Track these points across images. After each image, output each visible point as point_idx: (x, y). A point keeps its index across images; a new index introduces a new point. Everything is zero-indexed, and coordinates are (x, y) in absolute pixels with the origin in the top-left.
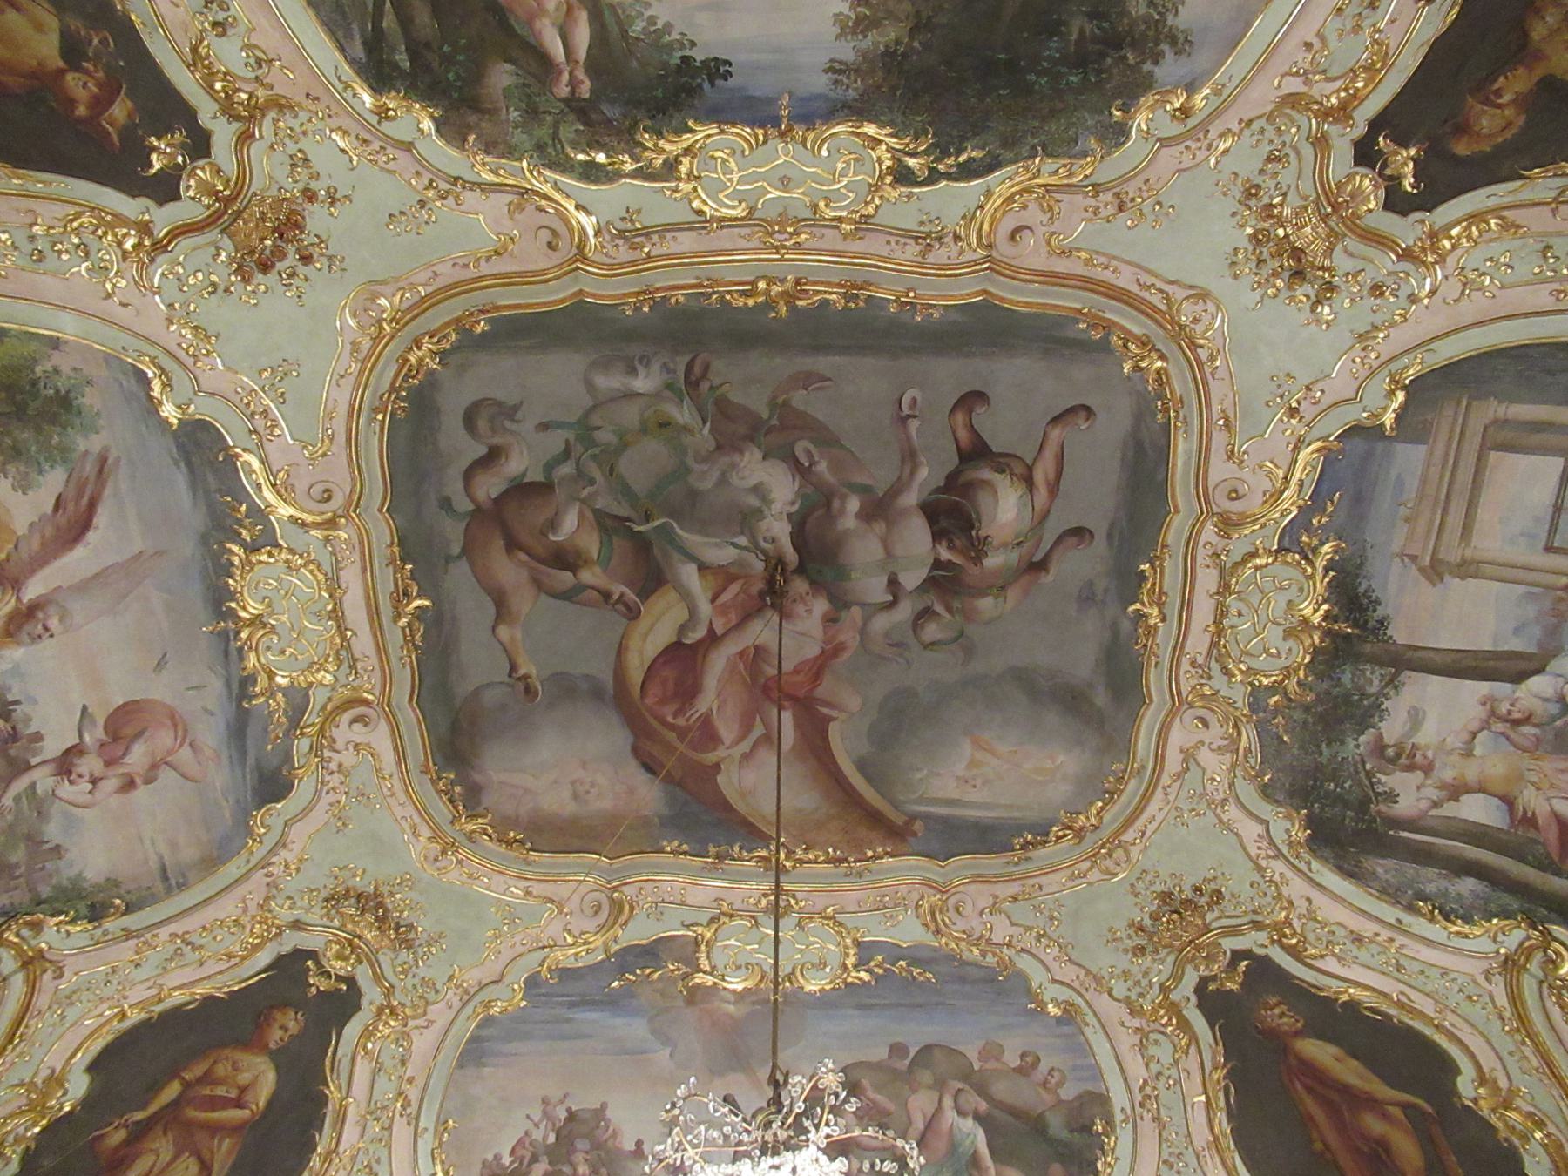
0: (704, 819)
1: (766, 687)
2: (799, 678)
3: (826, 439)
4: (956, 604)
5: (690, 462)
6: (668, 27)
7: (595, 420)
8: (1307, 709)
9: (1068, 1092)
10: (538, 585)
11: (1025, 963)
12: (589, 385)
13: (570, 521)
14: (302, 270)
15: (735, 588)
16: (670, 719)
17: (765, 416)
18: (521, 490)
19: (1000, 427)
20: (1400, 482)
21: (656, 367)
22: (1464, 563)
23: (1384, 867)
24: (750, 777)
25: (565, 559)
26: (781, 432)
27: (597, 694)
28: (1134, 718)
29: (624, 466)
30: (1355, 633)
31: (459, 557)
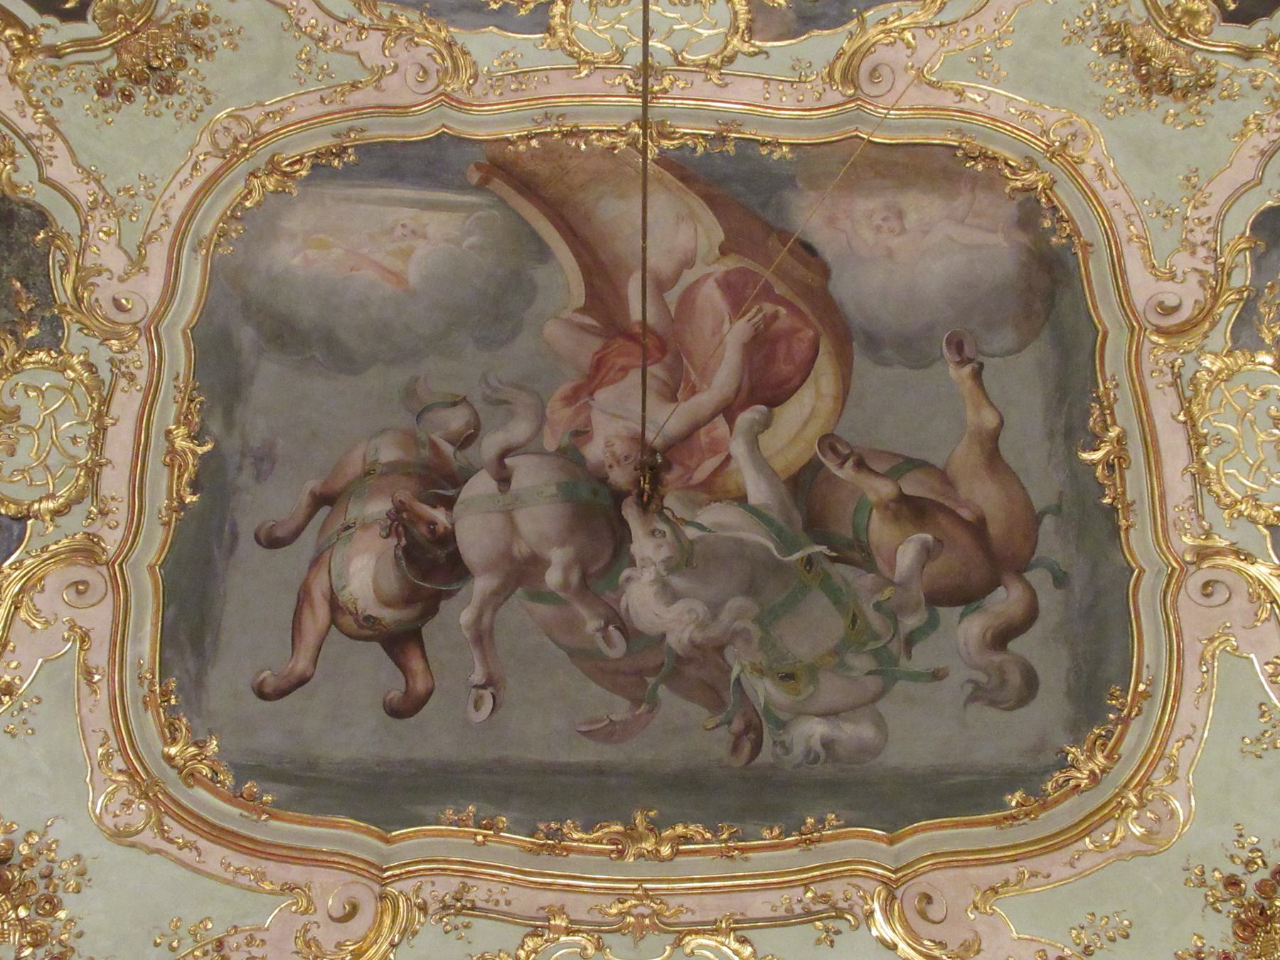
0: (739, 186)
1: (661, 351)
2: (621, 362)
3: (586, 659)
4: (426, 453)
5: (755, 630)
7: (873, 684)
10: (945, 478)
12: (880, 723)
13: (907, 556)
14: (1238, 870)
15: (701, 474)
16: (783, 311)
17: (663, 691)
18: (966, 596)
19: (371, 671)
21: (798, 750)
24: (683, 238)
25: (913, 511)
26: (642, 667)
27: (873, 343)
28: (206, 311)
29: (836, 626)
31: (1043, 513)
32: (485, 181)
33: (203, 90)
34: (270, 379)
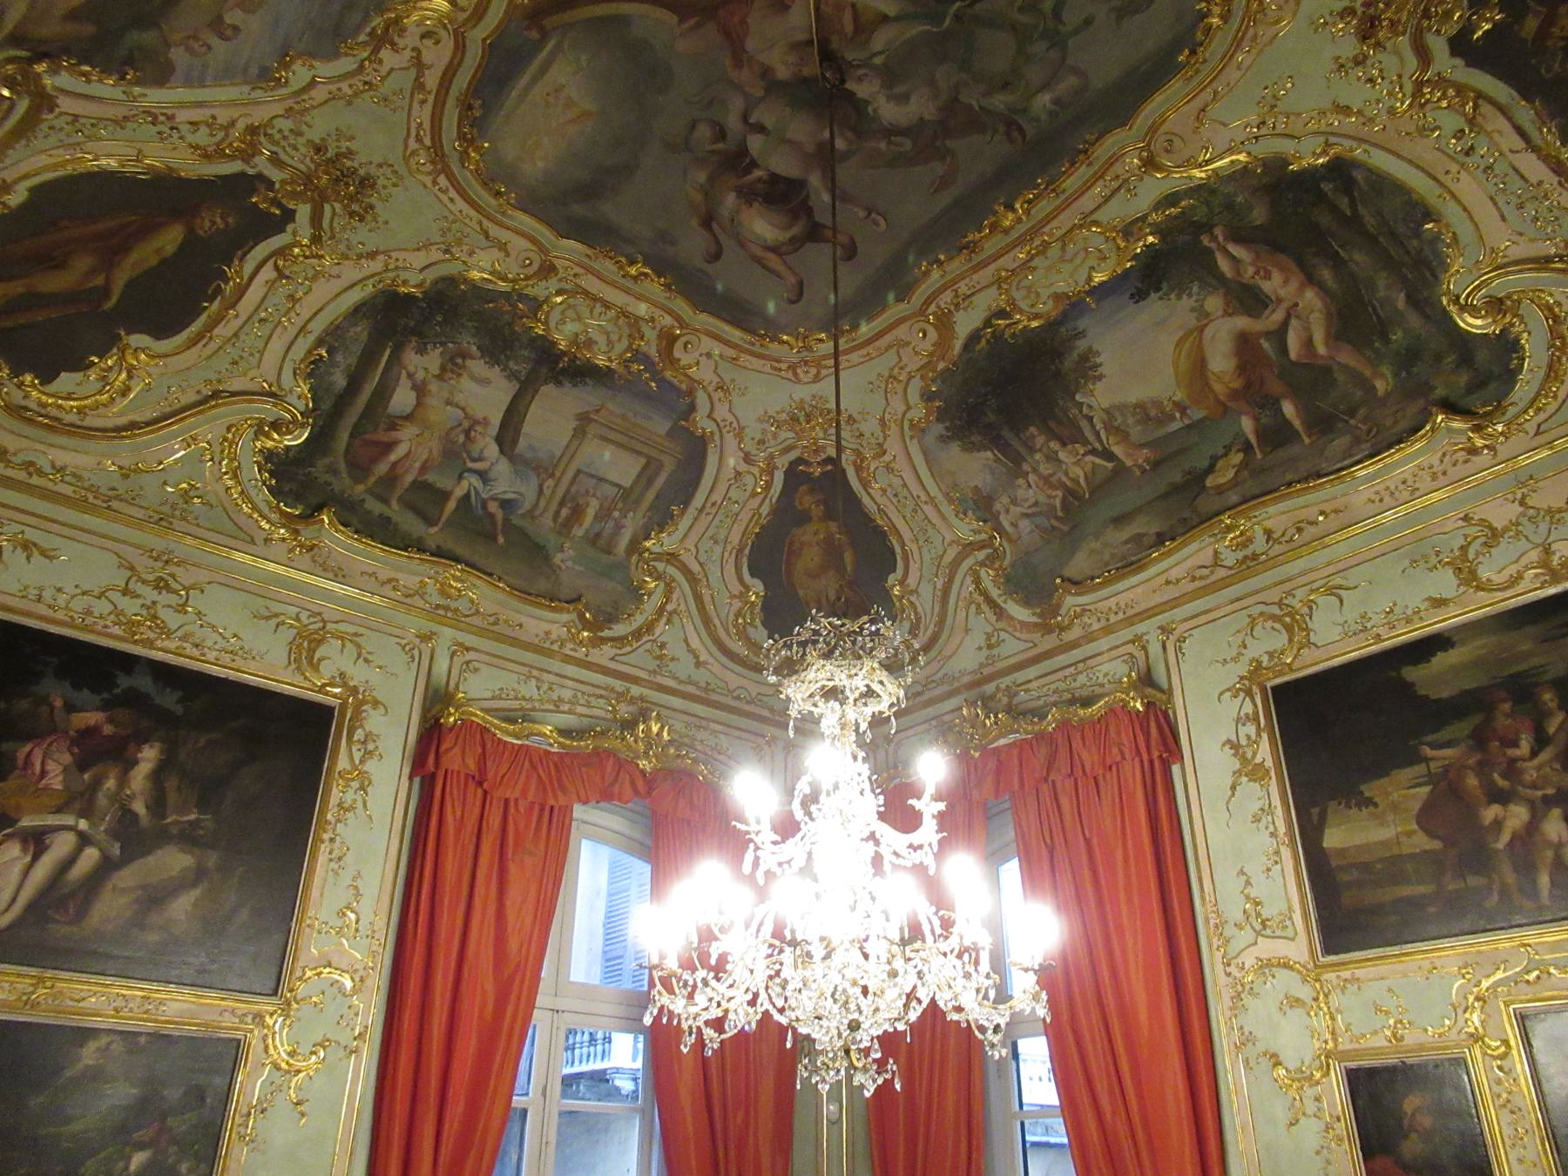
6: (1179, 297)
8: (510, 324)
9: (177, 55)
11: (346, 64)
12: (1075, 71)
15: (849, 27)
17: (948, 143)
19: (818, 257)
20: (649, 418)
21: (1043, 117)
22: (584, 433)
23: (361, 332)
26: (928, 141)
28: (550, 224)
30: (554, 366)
32: (541, 29)
33: (380, 166)
34: (610, 210)
